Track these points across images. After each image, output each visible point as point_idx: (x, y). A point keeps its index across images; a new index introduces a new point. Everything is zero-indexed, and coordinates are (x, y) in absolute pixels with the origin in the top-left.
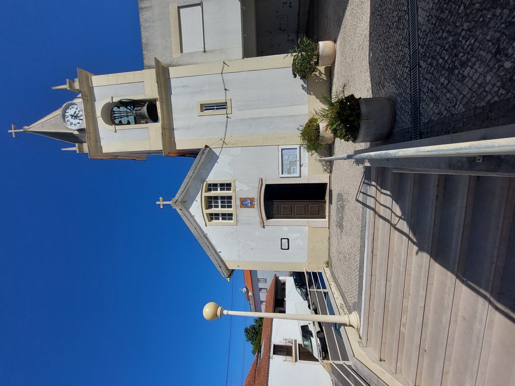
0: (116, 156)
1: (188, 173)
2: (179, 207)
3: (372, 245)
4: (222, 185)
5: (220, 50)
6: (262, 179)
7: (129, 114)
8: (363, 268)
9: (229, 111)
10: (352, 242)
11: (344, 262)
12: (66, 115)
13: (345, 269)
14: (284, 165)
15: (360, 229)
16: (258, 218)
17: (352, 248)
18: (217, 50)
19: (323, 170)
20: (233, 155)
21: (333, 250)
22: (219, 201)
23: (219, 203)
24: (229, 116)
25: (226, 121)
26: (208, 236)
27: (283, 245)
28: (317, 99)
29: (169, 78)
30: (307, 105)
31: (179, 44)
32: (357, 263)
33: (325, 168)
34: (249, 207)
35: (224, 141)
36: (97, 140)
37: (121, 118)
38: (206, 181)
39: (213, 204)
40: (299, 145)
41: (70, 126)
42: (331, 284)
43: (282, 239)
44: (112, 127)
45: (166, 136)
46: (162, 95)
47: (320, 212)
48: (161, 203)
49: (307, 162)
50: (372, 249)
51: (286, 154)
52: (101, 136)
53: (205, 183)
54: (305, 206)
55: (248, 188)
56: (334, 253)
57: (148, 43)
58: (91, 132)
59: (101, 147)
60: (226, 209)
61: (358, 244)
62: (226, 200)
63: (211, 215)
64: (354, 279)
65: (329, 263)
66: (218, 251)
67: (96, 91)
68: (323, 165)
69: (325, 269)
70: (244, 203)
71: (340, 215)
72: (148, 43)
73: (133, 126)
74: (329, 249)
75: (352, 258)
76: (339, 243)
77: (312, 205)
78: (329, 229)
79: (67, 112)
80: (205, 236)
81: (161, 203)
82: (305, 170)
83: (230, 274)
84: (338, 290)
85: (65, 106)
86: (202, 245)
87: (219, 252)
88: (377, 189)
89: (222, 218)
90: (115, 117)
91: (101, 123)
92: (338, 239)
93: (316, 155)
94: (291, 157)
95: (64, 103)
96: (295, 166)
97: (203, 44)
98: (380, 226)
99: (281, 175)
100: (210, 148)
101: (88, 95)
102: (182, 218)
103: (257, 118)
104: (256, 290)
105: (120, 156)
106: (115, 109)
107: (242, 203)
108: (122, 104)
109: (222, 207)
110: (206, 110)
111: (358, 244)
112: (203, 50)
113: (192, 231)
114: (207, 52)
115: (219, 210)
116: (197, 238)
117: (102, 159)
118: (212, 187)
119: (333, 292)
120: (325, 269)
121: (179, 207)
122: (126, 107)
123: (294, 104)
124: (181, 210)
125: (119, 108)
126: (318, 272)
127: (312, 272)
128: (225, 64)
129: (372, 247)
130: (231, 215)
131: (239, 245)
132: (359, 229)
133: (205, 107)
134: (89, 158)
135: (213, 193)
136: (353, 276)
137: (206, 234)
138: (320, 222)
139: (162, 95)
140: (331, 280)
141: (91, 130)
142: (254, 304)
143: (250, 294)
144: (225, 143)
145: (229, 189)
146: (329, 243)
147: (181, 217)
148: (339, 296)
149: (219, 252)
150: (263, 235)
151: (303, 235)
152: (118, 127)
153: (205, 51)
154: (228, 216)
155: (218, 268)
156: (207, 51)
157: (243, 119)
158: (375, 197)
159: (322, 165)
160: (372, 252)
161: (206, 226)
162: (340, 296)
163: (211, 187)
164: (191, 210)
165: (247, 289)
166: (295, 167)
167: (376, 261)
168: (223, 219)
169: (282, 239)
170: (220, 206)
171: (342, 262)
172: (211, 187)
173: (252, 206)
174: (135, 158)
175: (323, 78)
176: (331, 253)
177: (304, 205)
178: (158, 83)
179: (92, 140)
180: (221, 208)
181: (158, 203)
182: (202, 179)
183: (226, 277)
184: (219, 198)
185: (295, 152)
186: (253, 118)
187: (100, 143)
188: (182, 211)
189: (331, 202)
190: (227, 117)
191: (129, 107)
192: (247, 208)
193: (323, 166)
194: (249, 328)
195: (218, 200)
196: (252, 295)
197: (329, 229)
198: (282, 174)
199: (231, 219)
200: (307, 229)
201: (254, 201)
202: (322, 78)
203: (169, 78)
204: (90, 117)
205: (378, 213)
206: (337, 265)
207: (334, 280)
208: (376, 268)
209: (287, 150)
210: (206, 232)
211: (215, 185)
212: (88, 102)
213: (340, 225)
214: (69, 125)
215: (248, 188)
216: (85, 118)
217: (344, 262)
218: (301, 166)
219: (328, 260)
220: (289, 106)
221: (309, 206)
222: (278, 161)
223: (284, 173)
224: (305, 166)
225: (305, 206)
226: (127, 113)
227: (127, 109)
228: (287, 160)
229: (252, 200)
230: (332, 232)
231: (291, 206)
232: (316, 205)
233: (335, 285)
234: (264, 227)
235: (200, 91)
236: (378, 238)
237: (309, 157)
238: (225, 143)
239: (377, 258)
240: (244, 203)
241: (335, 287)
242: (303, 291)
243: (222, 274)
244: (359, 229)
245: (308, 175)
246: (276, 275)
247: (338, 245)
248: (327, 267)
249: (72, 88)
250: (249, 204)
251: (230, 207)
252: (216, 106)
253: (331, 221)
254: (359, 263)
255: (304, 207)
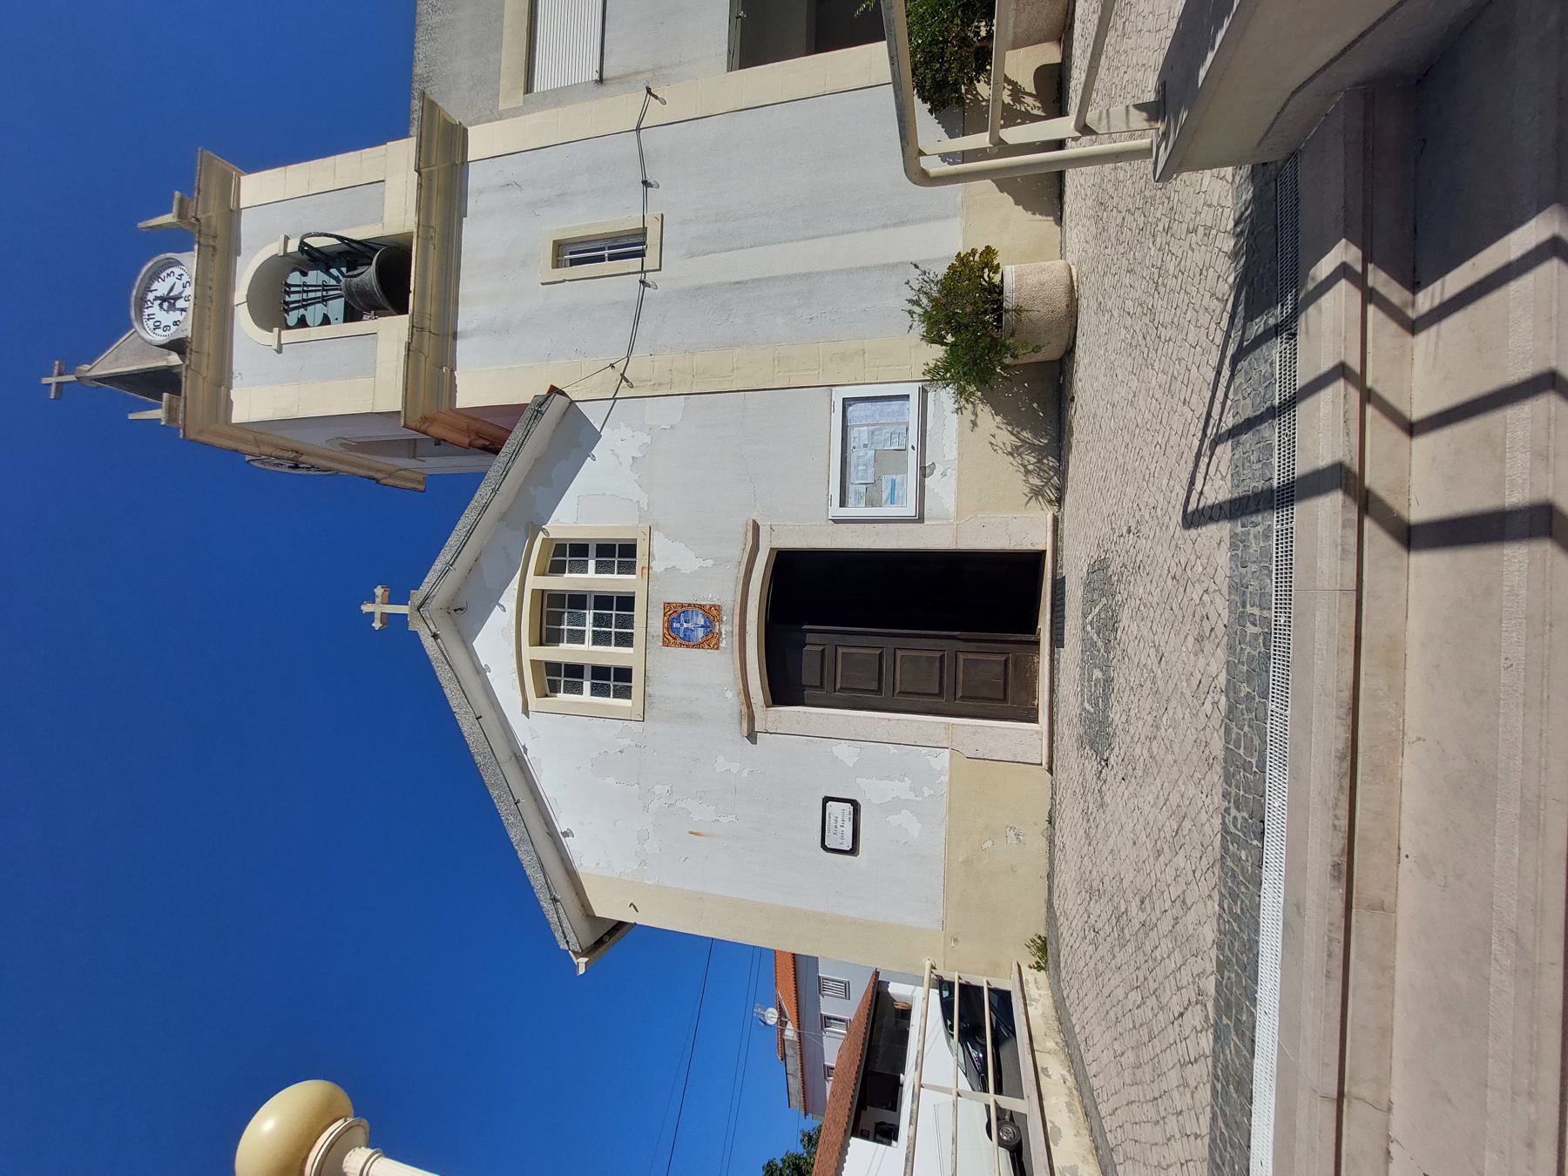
0: (297, 452)
1: (475, 493)
2: (432, 627)
3: (1336, 806)
4: (605, 550)
5: (653, 70)
6: (756, 528)
7: (331, 293)
8: (1252, 1015)
9: (651, 259)
10: (1162, 818)
11: (1112, 948)
12: (148, 298)
13: (1120, 993)
14: (852, 469)
15: (1215, 704)
16: (729, 695)
17: (1159, 853)
18: (642, 72)
19: (1027, 491)
20: (650, 429)
21: (1066, 877)
22: (589, 615)
23: (587, 623)
24: (650, 277)
25: (635, 296)
26: (530, 757)
27: (833, 829)
28: (1002, 192)
29: (465, 163)
30: (959, 219)
31: (1334, 1148)
32: (1196, 966)
33: (1037, 482)
34: (699, 646)
35: (622, 375)
36: (223, 378)
37: (304, 307)
38: (543, 530)
39: (565, 627)
40: (920, 384)
41: (152, 334)
42: (1045, 1070)
43: (826, 800)
44: (270, 338)
45: (424, 357)
46: (428, 217)
47: (1009, 692)
48: (378, 608)
49: (954, 454)
50: (1340, 843)
51: (864, 422)
52: (235, 367)
53: (541, 535)
54: (942, 657)
55: (700, 563)
56: (1069, 892)
57: (431, 74)
58: (205, 350)
59: (229, 405)
60: (612, 649)
61: (1204, 817)
62: (614, 613)
63: (553, 668)
64: (1173, 1078)
65: (1049, 947)
66: (561, 826)
67: (247, 224)
68: (1025, 467)
69: (1029, 975)
70: (678, 625)
71: (1097, 674)
72: (431, 74)
73: (340, 328)
74: (1050, 877)
75: (1165, 926)
76: (1093, 831)
77: (970, 656)
78: (1050, 770)
79: (152, 289)
80: (519, 758)
81: (378, 608)
82: (942, 490)
83: (599, 943)
84: (1080, 1114)
85: (149, 269)
86: (494, 793)
87: (566, 834)
88: (1370, 296)
89: (592, 684)
90: (287, 303)
91: (243, 317)
92: (1085, 812)
93: (988, 420)
94: (885, 433)
95: (150, 260)
96: (897, 474)
97: (598, 56)
98: (1415, 629)
99: (837, 511)
100: (572, 402)
101: (218, 233)
102: (435, 673)
103: (753, 281)
104: (811, 1023)
105: (308, 454)
106: (295, 278)
107: (672, 626)
108: (312, 258)
109: (599, 639)
110: (574, 262)
111: (1204, 817)
112: (596, 77)
113: (465, 729)
114: (609, 82)
115: (586, 652)
116: (478, 759)
117: (236, 451)
118: (568, 559)
119: (1049, 1125)
120: (1029, 975)
121: (432, 627)
122: (327, 272)
123: (905, 220)
124: (435, 636)
125: (304, 274)
126: (993, 986)
127: (960, 985)
128: (654, 95)
129: (1344, 823)
130: (624, 674)
131: (646, 808)
132: (1208, 707)
133: (571, 253)
134: (181, 436)
135: (568, 582)
136: (1169, 1059)
137: (524, 747)
138: (1005, 735)
139: (428, 217)
140: (1048, 1043)
141: (209, 345)
142: (799, 1075)
143: (790, 1033)
144: (627, 381)
145: (629, 568)
146: (1051, 842)
147: (432, 666)
148: (1085, 1160)
149: (566, 834)
150: (745, 774)
151: (927, 792)
152: (287, 336)
153: (601, 81)
154: (613, 680)
155: (546, 905)
156: (607, 80)
157: (700, 288)
158: (1357, 369)
159: (1023, 470)
160: (1346, 871)
161: (526, 711)
162: (1090, 1157)
163: (565, 556)
164: (478, 644)
165: (781, 1013)
166: (898, 478)
167: (1387, 969)
168: (597, 691)
169: (826, 800)
170: (589, 636)
171: (1103, 950)
172: (565, 556)
173: (710, 640)
174: (378, 476)
175: (1029, 109)
176: (1056, 895)
177: (938, 655)
178: (420, 174)
179: (204, 378)
180: (594, 644)
181: (366, 608)
182: (532, 523)
183: (573, 952)
184: (591, 602)
185: (903, 414)
186: (739, 283)
187: (229, 388)
188: (439, 640)
189: (1057, 640)
190: (642, 282)
191: (334, 271)
192: (688, 646)
193: (1027, 472)
194: (780, 1165)
195: (585, 609)
196: (796, 1039)
197: (1050, 770)
198: (843, 504)
199: (625, 693)
200: (947, 764)
201: (720, 621)
202: (1023, 109)
203: (463, 163)
204: (211, 301)
205: (1389, 510)
206: (1082, 963)
207: (1068, 1046)
208: (1386, 1032)
209: (868, 405)
210: (523, 738)
211: (580, 549)
212: (213, 256)
213: (1098, 736)
214: (149, 332)
215: (700, 563)
216: (195, 304)
217: (1112, 948)
218: (923, 472)
219: (1043, 934)
220: (885, 226)
221: (961, 657)
222: (828, 450)
223: (851, 500)
224: (944, 475)
225: (942, 657)
226: (324, 290)
227: (326, 278)
228: (865, 446)
229: (712, 614)
230: (1063, 784)
231: (881, 654)
232: (992, 657)
233: (1067, 1075)
234: (752, 736)
235: (559, 195)
236: (1396, 742)
237: (961, 434)
238: (627, 381)
239: (1388, 939)
240: (678, 625)
241: (1065, 1090)
242: (974, 1055)
243: (559, 935)
244: (1208, 707)
245: (957, 513)
246: (877, 974)
247: (1086, 846)
248: (1039, 968)
249: (186, 218)
250: (700, 633)
251: (625, 640)
252: (610, 248)
253: (1062, 727)
254: (1211, 966)
255: (937, 665)
